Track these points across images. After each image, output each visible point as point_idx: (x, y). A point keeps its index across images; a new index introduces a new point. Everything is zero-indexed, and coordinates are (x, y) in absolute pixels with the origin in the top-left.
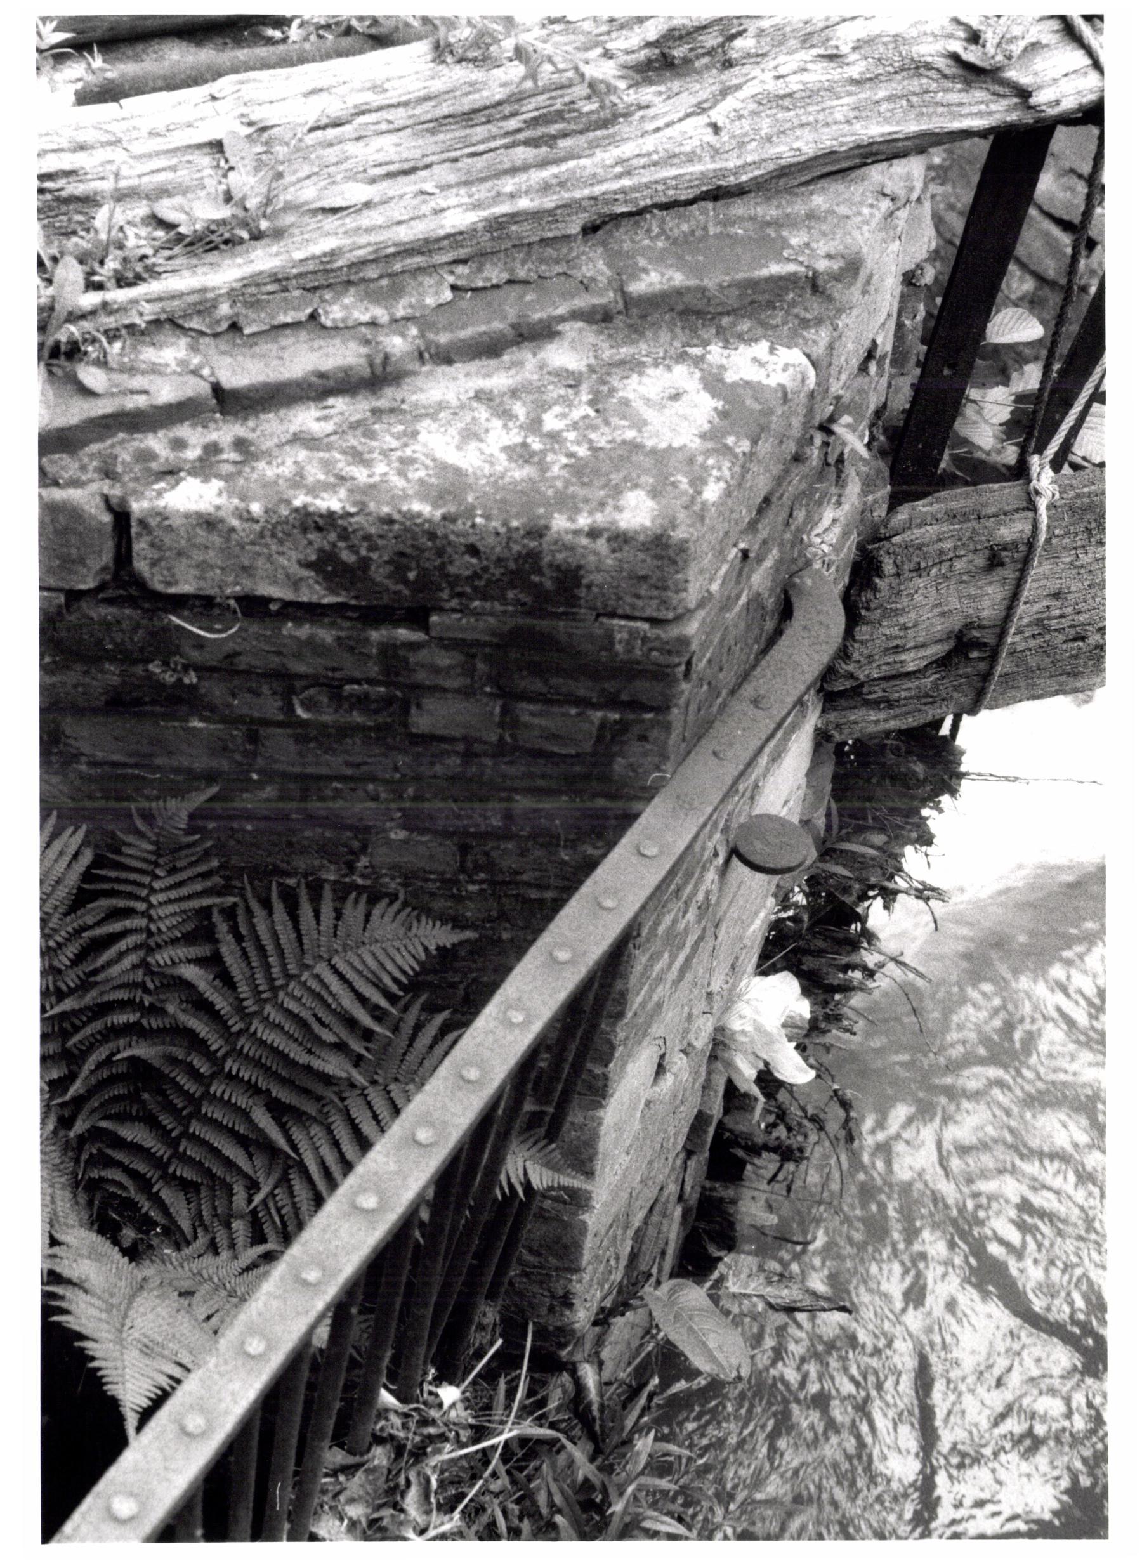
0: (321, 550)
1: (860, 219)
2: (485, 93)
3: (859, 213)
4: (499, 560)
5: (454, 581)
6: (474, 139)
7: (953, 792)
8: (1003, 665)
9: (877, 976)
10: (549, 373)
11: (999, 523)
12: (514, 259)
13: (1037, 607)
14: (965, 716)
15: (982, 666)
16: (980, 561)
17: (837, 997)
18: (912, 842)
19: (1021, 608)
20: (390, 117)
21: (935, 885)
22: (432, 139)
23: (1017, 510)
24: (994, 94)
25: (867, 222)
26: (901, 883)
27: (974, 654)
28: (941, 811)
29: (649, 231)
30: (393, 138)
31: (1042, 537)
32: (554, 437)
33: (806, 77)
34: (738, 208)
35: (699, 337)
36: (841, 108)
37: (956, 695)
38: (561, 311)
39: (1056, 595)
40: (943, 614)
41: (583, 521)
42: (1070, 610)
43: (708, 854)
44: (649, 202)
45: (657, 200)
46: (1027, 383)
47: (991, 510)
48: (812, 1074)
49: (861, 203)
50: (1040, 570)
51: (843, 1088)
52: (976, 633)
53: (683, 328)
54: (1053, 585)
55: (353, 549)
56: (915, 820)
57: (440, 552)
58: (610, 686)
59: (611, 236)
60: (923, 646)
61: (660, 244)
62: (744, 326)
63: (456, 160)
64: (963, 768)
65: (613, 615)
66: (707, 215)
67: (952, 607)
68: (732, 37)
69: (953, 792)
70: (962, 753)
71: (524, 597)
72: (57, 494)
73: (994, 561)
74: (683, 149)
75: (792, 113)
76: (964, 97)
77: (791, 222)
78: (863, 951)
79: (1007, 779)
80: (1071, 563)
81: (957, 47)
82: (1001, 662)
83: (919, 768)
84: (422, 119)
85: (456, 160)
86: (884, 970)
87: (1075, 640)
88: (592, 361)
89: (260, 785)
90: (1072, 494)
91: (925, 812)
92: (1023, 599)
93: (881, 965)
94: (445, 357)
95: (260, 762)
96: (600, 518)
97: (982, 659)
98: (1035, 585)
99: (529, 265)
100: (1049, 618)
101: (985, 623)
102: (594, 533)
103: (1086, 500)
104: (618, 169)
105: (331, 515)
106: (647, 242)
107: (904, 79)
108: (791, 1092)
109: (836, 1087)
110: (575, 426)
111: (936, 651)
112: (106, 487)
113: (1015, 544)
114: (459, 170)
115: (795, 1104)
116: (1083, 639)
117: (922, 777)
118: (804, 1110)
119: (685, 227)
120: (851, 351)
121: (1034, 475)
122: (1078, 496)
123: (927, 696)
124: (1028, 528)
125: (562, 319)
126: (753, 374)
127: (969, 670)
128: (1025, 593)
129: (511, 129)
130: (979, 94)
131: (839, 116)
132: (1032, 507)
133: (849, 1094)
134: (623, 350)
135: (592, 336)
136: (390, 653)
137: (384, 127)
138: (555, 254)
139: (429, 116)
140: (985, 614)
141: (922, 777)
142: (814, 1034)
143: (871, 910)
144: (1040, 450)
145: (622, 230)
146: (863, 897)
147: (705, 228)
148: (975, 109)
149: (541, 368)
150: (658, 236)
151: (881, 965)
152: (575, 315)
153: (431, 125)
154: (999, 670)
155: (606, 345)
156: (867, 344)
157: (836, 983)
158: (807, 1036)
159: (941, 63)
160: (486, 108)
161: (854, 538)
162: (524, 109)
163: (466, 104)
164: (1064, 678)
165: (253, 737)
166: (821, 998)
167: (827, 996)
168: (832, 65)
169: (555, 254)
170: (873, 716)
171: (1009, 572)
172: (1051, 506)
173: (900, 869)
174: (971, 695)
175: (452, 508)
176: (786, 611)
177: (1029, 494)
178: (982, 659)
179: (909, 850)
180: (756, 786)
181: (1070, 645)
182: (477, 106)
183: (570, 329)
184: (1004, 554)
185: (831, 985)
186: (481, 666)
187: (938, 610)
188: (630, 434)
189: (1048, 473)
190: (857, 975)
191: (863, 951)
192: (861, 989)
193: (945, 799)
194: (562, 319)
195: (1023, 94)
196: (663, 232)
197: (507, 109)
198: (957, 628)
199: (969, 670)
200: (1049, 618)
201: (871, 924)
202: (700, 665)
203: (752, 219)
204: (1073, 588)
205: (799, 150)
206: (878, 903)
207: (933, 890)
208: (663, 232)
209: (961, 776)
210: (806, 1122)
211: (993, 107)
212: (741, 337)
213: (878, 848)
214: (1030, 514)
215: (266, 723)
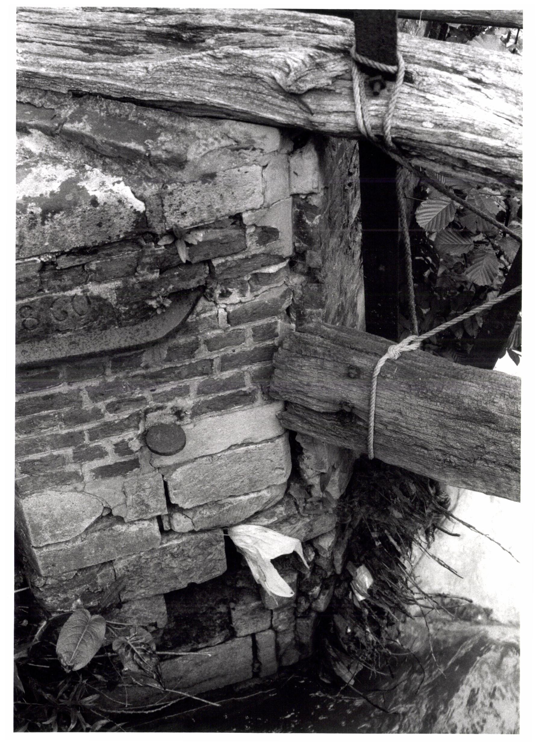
1: (205, 142)
2: (78, 21)
3: (206, 140)
6: (62, 39)
10: (23, 149)
12: (36, 95)
20: (32, 17)
22: (43, 32)
24: (301, 108)
25: (206, 145)
29: (101, 106)
30: (27, 25)
33: (200, 63)
35: (93, 162)
36: (210, 83)
38: (32, 123)
44: (96, 91)
45: (102, 92)
49: (212, 136)
53: (87, 154)
59: (85, 102)
61: (102, 114)
62: (116, 167)
63: (44, 44)
66: (132, 110)
74: (125, 74)
75: (186, 78)
76: (284, 104)
84: (44, 22)
85: (44, 44)
88: (44, 152)
92: (81, 353)
99: (43, 100)
104: (91, 72)
106: (98, 111)
107: (249, 82)
114: (42, 48)
119: (118, 111)
125: (32, 127)
129: (83, 40)
130: (292, 105)
131: (206, 87)
134: (59, 153)
135: (45, 140)
137: (28, 20)
138: (56, 100)
139: (47, 21)
145: (90, 101)
147: (127, 116)
148: (288, 112)
149: (21, 145)
150: (104, 110)
152: (37, 127)
153: (47, 26)
155: (52, 147)
160: (76, 27)
162: (97, 35)
163: (67, 22)
168: (214, 61)
169: (56, 100)
182: (71, 24)
183: (36, 133)
194: (32, 127)
196: (107, 109)
197: (88, 32)
203: (155, 121)
205: (173, 94)
208: (107, 109)
211: (299, 115)
212: (111, 171)
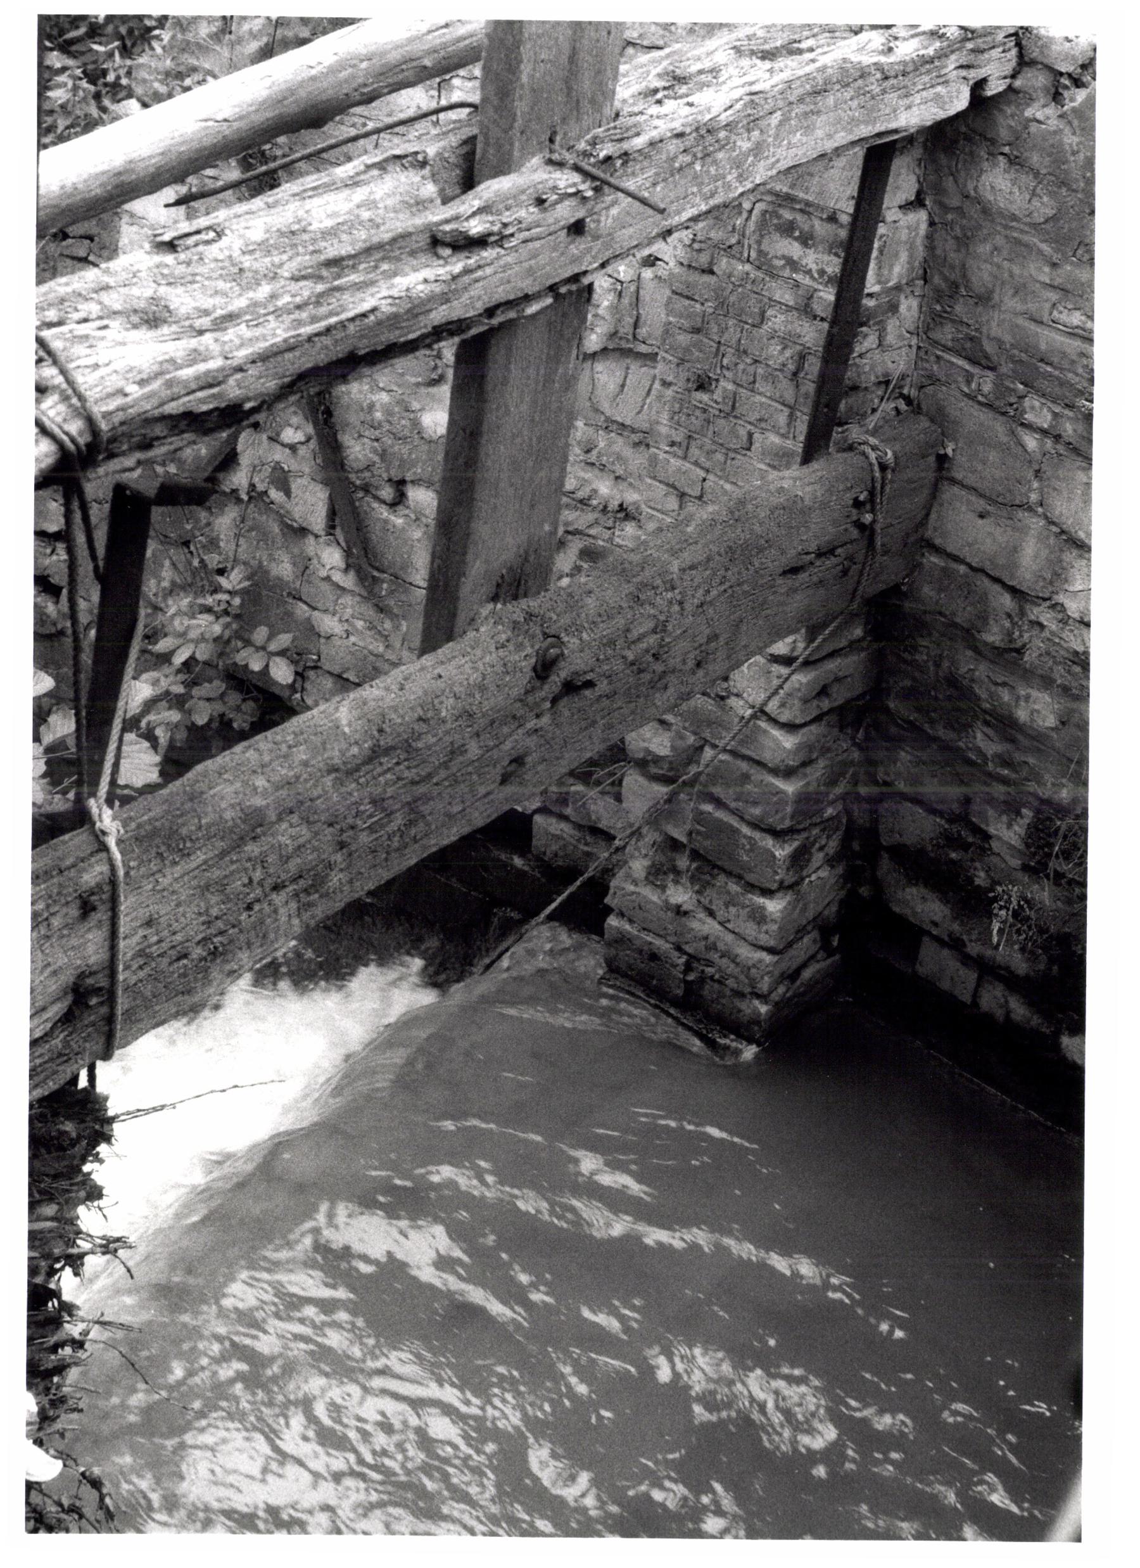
7: (108, 1139)
8: (122, 1003)
9: (87, 1346)
11: (79, 872)
13: (136, 939)
14: (99, 1064)
15: (104, 1010)
16: (74, 912)
17: (56, 1379)
18: (83, 1202)
19: (122, 944)
21: (116, 1234)
23: (92, 854)
26: (84, 1245)
27: (93, 1001)
28: (101, 1161)
31: (121, 873)
37: (87, 1045)
39: (149, 923)
40: (55, 973)
42: (166, 933)
46: (54, 733)
47: (69, 862)
48: (58, 1465)
50: (128, 903)
51: (89, 1468)
52: (90, 981)
54: (143, 914)
56: (80, 1178)
64: (111, 1113)
67: (60, 963)
69: (108, 1139)
70: (106, 1099)
73: (86, 908)
78: (66, 1325)
79: (155, 1109)
80: (153, 890)
82: (120, 1001)
83: (69, 1127)
86: (90, 1337)
87: (178, 959)
90: (133, 825)
91: (86, 1168)
92: (121, 935)
93: (86, 1333)
97: (101, 1003)
98: (128, 919)
100: (149, 946)
101: (95, 968)
103: (148, 828)
108: (41, 1491)
109: (82, 1469)
113: (99, 886)
115: (48, 1501)
116: (185, 956)
117: (74, 1135)
118: (60, 1504)
121: (96, 818)
122: (139, 826)
123: (60, 1055)
124: (105, 868)
127: (92, 1018)
128: (122, 930)
132: (104, 848)
133: (96, 1471)
140: (92, 960)
141: (74, 1135)
142: (45, 1425)
143: (62, 1283)
144: (93, 794)
146: (52, 1272)
151: (86, 1333)
154: (119, 1010)
157: (50, 1366)
158: (40, 1429)
164: (180, 998)
166: (41, 1388)
167: (47, 1382)
171: (101, 915)
172: (119, 842)
173: (79, 1232)
174: (102, 1040)
177: (97, 836)
178: (101, 1003)
179: (81, 1210)
181: (176, 965)
184: (93, 898)
185: (47, 1370)
187: (49, 970)
189: (107, 813)
190: (68, 1350)
191: (66, 1325)
192: (76, 1364)
193: (103, 1149)
198: (72, 979)
199: (92, 1018)
200: (149, 946)
201: (66, 1297)
204: (162, 912)
206: (68, 1271)
207: (118, 1240)
209: (112, 1120)
210: (63, 1516)
213: (52, 1219)
214: (104, 855)
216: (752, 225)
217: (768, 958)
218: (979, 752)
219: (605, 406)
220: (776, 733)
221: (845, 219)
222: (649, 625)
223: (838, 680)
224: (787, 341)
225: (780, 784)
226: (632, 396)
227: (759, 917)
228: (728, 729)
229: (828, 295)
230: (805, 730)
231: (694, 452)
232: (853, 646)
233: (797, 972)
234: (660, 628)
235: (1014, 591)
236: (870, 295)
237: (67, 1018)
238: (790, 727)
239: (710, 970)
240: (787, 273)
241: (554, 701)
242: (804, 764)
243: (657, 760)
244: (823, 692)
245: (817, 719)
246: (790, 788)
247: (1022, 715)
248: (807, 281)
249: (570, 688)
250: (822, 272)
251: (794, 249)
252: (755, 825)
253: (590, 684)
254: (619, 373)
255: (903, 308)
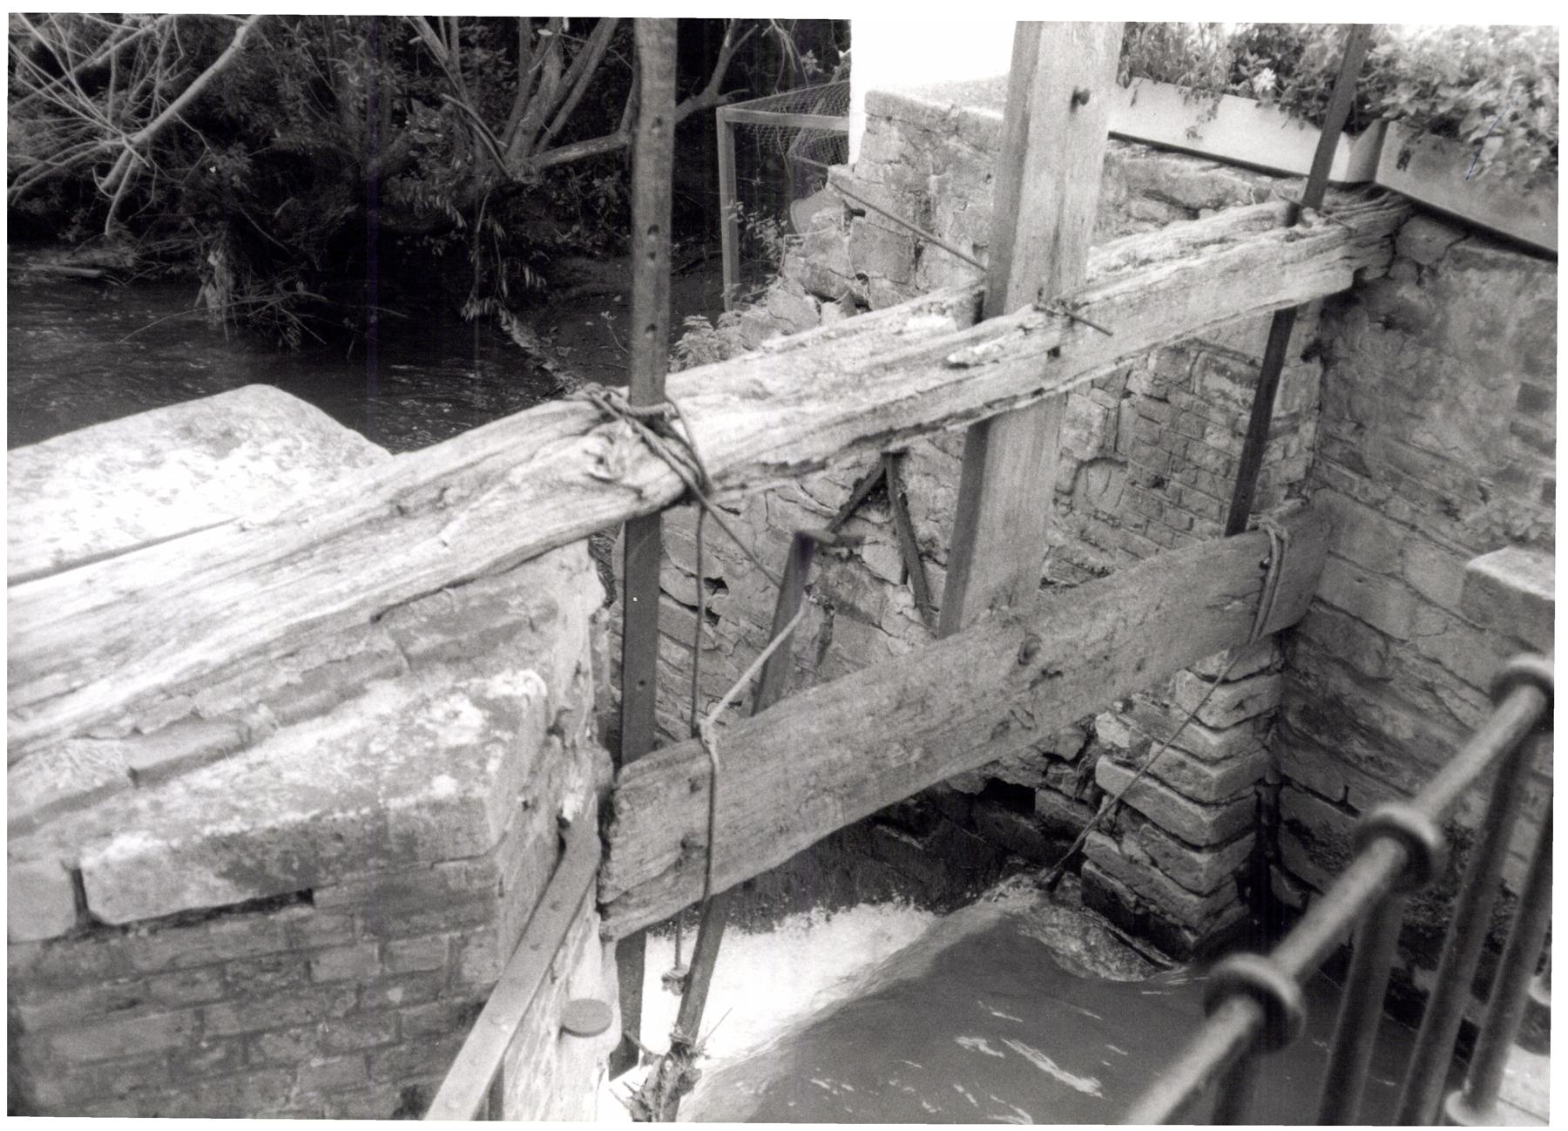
0: (232, 863)
4: (358, 839)
5: (326, 863)
16: (686, 789)
32: (380, 756)
33: (498, 503)
34: (472, 590)
41: (411, 800)
43: (543, 1032)
55: (252, 856)
57: (313, 844)
58: (450, 913)
60: (660, 856)
65: (442, 860)
68: (444, 490)
71: (382, 863)
72: (22, 867)
73: (694, 788)
77: (512, 593)
81: (591, 468)
89: (211, 1049)
94: (290, 721)
95: (208, 1033)
96: (421, 797)
102: (418, 806)
105: (232, 837)
110: (392, 746)
111: (669, 858)
112: (60, 854)
120: (564, 673)
126: (506, 690)
132: (707, 751)
136: (293, 929)
156: (574, 664)
159: (582, 480)
161: (594, 797)
165: (200, 1015)
170: (636, 914)
172: (718, 746)
175: (316, 812)
176: (562, 846)
180: (568, 982)
186: (359, 923)
188: (429, 744)
195: (639, 492)
202: (509, 887)
215: (207, 1002)
216: (1197, 367)
217: (1194, 899)
218: (1357, 756)
219: (1094, 500)
220: (1205, 733)
221: (1260, 363)
222: (1101, 635)
223: (1251, 697)
224: (1219, 452)
225: (1206, 769)
226: (1113, 492)
227: (1192, 866)
228: (1170, 730)
229: (1246, 418)
230: (1227, 733)
231: (1151, 531)
232: (1263, 671)
233: (1218, 914)
234: (1109, 638)
235: (1382, 634)
236: (1278, 419)
237: (678, 864)
238: (1215, 730)
239: (1153, 908)
240: (1220, 401)
241: (1034, 684)
242: (1225, 758)
243: (1119, 750)
244: (1240, 706)
245: (1237, 724)
246: (1215, 773)
247: (1387, 729)
248: (1234, 407)
249: (1047, 674)
250: (1244, 401)
251: (1226, 385)
252: (1189, 798)
253: (1058, 673)
254: (1105, 477)
255: (1302, 430)
